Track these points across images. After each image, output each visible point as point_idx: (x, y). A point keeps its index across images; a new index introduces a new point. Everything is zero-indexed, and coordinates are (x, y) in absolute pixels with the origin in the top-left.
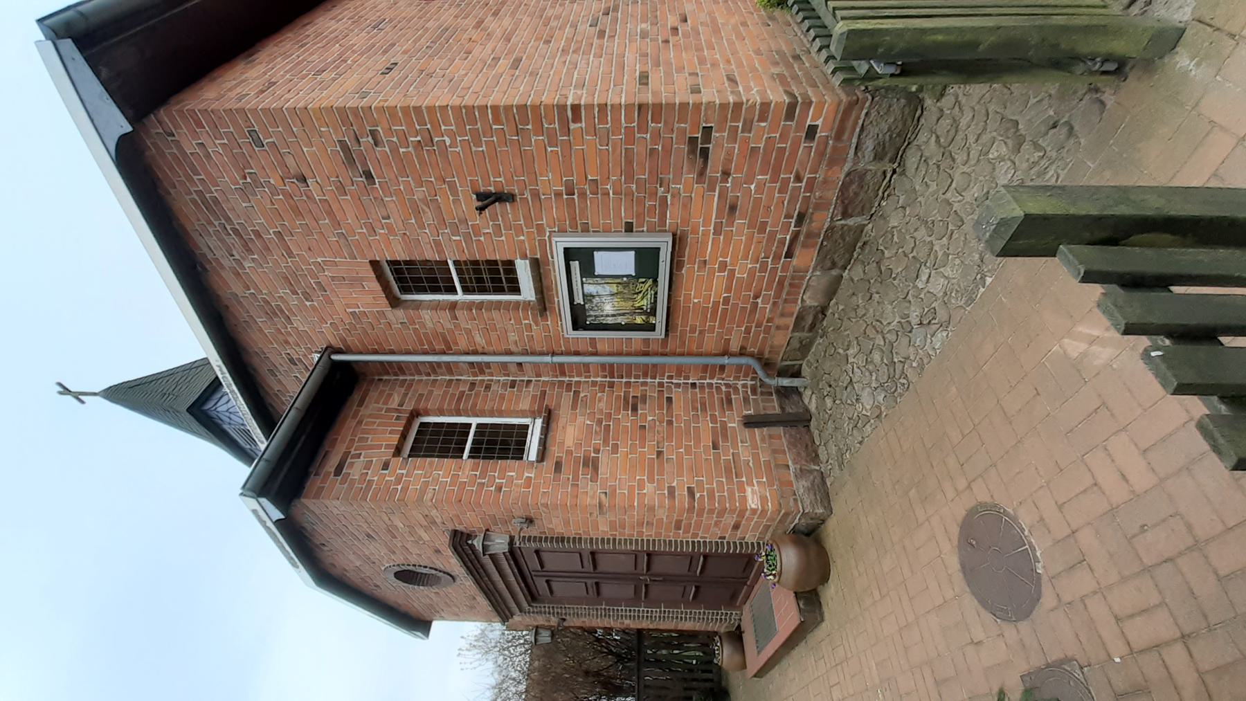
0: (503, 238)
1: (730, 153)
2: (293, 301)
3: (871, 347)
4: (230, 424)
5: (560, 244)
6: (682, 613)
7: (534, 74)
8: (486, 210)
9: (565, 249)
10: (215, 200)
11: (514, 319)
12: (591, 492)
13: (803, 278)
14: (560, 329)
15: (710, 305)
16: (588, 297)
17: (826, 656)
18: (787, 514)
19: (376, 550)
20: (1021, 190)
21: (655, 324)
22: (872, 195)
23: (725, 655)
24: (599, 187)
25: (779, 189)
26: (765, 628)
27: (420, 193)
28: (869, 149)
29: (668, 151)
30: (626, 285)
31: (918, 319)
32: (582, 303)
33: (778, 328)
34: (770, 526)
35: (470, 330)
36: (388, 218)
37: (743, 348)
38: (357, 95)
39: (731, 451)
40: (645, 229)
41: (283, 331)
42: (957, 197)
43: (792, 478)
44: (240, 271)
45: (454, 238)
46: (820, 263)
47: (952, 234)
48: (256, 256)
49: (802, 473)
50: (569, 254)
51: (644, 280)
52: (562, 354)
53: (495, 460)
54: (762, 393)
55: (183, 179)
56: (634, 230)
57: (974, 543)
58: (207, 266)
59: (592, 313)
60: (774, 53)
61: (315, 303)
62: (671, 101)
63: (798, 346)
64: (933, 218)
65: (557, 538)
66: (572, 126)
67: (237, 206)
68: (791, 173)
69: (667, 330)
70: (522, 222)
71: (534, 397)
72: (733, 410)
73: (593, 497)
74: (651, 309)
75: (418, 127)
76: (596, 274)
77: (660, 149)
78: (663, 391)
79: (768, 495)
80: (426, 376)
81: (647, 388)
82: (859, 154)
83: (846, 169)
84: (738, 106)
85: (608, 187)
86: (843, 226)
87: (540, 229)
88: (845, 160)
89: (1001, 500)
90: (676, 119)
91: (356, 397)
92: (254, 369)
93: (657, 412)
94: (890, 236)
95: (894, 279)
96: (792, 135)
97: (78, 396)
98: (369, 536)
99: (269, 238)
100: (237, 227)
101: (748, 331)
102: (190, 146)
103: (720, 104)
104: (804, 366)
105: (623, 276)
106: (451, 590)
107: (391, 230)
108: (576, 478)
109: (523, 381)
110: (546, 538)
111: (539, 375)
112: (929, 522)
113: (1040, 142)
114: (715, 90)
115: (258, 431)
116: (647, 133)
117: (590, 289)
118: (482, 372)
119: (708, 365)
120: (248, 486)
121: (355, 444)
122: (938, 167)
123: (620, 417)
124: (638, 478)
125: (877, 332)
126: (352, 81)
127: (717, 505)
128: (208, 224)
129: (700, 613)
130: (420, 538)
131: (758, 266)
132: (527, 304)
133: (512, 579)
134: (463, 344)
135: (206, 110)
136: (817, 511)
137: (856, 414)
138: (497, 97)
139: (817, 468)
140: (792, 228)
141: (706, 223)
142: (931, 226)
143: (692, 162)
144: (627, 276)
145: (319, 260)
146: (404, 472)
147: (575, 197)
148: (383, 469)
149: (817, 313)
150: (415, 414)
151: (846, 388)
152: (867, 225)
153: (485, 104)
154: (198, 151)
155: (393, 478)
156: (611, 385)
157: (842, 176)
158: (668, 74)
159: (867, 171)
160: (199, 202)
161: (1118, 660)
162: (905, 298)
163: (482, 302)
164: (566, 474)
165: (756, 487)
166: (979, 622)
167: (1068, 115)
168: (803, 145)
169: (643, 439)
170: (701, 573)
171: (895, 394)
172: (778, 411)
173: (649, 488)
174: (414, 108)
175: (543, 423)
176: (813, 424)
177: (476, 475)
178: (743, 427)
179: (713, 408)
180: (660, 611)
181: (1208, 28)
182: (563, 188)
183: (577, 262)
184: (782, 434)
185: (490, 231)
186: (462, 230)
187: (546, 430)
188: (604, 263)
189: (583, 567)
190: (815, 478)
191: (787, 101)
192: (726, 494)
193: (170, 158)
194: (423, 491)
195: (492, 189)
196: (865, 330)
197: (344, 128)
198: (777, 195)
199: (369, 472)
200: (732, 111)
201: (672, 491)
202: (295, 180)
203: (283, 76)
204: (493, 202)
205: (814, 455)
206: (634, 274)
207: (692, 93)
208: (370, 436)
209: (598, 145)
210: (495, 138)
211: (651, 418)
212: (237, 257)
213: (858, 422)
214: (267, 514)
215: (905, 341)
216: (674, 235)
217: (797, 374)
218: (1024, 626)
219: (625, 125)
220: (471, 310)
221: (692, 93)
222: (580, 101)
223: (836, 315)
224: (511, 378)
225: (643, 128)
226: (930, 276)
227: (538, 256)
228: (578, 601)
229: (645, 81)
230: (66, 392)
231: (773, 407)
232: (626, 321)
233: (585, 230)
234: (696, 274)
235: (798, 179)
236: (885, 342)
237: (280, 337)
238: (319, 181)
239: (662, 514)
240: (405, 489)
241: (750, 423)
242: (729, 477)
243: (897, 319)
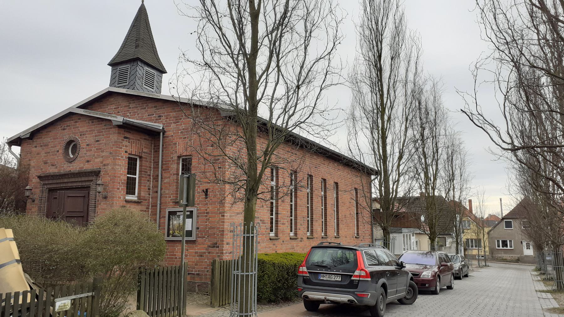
1: (213, 253)
16: (179, 216)
35: (170, 179)
52: (160, 207)
59: (174, 217)
66: (221, 215)
71: (145, 197)
76: (268, 120)
84: (222, 253)
91: (147, 137)
111: (152, 198)
117: (181, 217)
118: (154, 179)
134: (165, 175)
141: (198, 249)
146: (124, 158)
188: (189, 221)
195: (208, 193)
208: (135, 145)
216: (195, 241)
233: (198, 216)
240: (119, 159)
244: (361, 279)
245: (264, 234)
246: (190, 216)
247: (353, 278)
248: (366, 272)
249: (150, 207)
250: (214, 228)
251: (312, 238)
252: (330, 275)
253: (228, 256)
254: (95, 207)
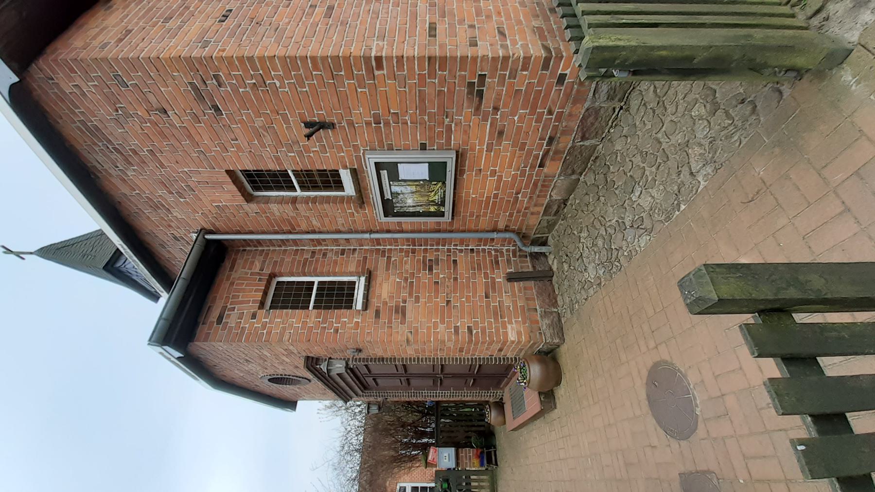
0: (328, 154)
1: (499, 95)
2: (171, 199)
3: (596, 235)
4: (137, 276)
5: (371, 159)
6: (465, 393)
7: (344, 23)
8: (314, 136)
9: (376, 163)
10: (96, 128)
11: (341, 209)
12: (401, 332)
13: (551, 181)
14: (375, 215)
15: (484, 199)
16: (395, 195)
17: (557, 430)
18: (534, 344)
19: (253, 367)
20: (717, 270)
21: (444, 212)
22: (604, 124)
23: (492, 417)
24: (400, 118)
25: (536, 120)
26: (519, 408)
27: (259, 122)
28: (604, 92)
29: (451, 92)
30: (422, 186)
31: (630, 223)
32: (391, 198)
33: (532, 214)
34: (523, 349)
35: (307, 216)
36: (237, 140)
37: (506, 226)
38: (200, 44)
39: (498, 299)
40: (435, 148)
41: (166, 219)
42: (666, 139)
43: (539, 319)
44: (126, 178)
45: (290, 154)
46: (564, 172)
47: (659, 166)
48: (136, 168)
49: (545, 314)
50: (379, 166)
51: (435, 183)
52: (377, 232)
53: (333, 310)
54: (520, 256)
55: (67, 111)
56: (427, 148)
57: (657, 384)
58: (99, 175)
59: (398, 205)
60: (535, 4)
61: (188, 200)
62: (454, 55)
63: (546, 225)
64: (647, 150)
65: (379, 359)
66: (377, 73)
67: (114, 132)
68: (545, 109)
69: (453, 215)
70: (342, 143)
72: (499, 269)
73: (402, 335)
74: (441, 202)
75: (252, 73)
76: (400, 179)
77: (446, 90)
78: (450, 255)
79: (522, 330)
80: (278, 247)
81: (439, 253)
82: (596, 95)
83: (587, 105)
84: (506, 59)
85: (407, 118)
86: (581, 146)
87: (356, 148)
88: (585, 100)
89: (678, 364)
90: (458, 69)
91: (227, 264)
92: (148, 244)
93: (446, 271)
94: (615, 157)
95: (616, 189)
96: (547, 81)
97: (18, 254)
98: (247, 360)
99: (144, 155)
100: (117, 146)
101: (511, 215)
102: (68, 88)
103: (492, 58)
104: (550, 238)
105: (421, 180)
106: (309, 386)
107: (239, 147)
108: (390, 322)
109: (350, 249)
110: (372, 359)
112: (628, 363)
113: (730, 112)
114: (488, 43)
115: (158, 285)
116: (435, 79)
119: (482, 239)
120: (153, 339)
121: (230, 300)
122: (654, 112)
123: (421, 275)
124: (433, 320)
125: (601, 225)
126: (194, 28)
127: (487, 339)
128: (93, 144)
129: (476, 393)
130: (284, 361)
131: (519, 172)
132: (350, 198)
133: (350, 380)
134: (304, 226)
135: (76, 59)
136: (555, 341)
137: (584, 279)
138: (314, 48)
139: (556, 310)
140: (544, 147)
142: (645, 156)
143: (470, 100)
144: (423, 180)
145: (185, 170)
146: (267, 320)
147: (382, 125)
148: (252, 319)
149: (561, 203)
150: (272, 276)
151: (578, 260)
152: (598, 145)
153: (305, 55)
154: (75, 90)
155: (260, 325)
156: (414, 251)
157: (583, 111)
158: (452, 26)
159: (601, 107)
160: (84, 129)
161: (742, 481)
162: (623, 205)
163: (316, 197)
164: (384, 319)
165: (514, 325)
166: (656, 434)
167: (753, 96)
168: (554, 88)
169: (437, 291)
170: (477, 372)
171: (612, 272)
172: (531, 269)
173: (441, 328)
174: (248, 58)
175: (366, 279)
176: (555, 279)
177: (319, 321)
179: (485, 267)
180: (451, 393)
181: (870, 55)
182: (372, 119)
183: (386, 171)
184: (533, 286)
185: (318, 149)
186: (295, 148)
187: (368, 287)
188: (405, 172)
189: (397, 371)
190: (554, 317)
191: (544, 56)
192: (493, 330)
193: (53, 96)
194: (282, 334)
196: (593, 222)
197: (192, 74)
198: (534, 124)
199: (242, 321)
200: (502, 63)
201: (457, 329)
202: (157, 112)
203: (137, 23)
204: (318, 130)
205: (554, 301)
206: (428, 179)
207: (470, 46)
208: (241, 294)
209: (398, 88)
210: (315, 82)
211: (442, 276)
212: (121, 168)
213: (585, 285)
214: (170, 354)
215: (620, 236)
216: (457, 152)
217: (544, 243)
218: (684, 443)
219: (418, 73)
220: (308, 203)
221: (470, 46)
222: (382, 52)
223: (574, 206)
224: (341, 248)
225: (432, 74)
226: (641, 193)
227: (356, 167)
228: (396, 388)
229: (433, 33)
230: (9, 252)
231: (528, 266)
232: (423, 210)
233: (391, 148)
234: (474, 178)
235: (550, 113)
236: (606, 233)
237: (164, 222)
238: (177, 112)
239: (450, 345)
240: (269, 333)
241: (511, 278)
242: (496, 319)
243: (616, 219)
246: (392, 169)
249: (382, 247)
254: (383, 359)
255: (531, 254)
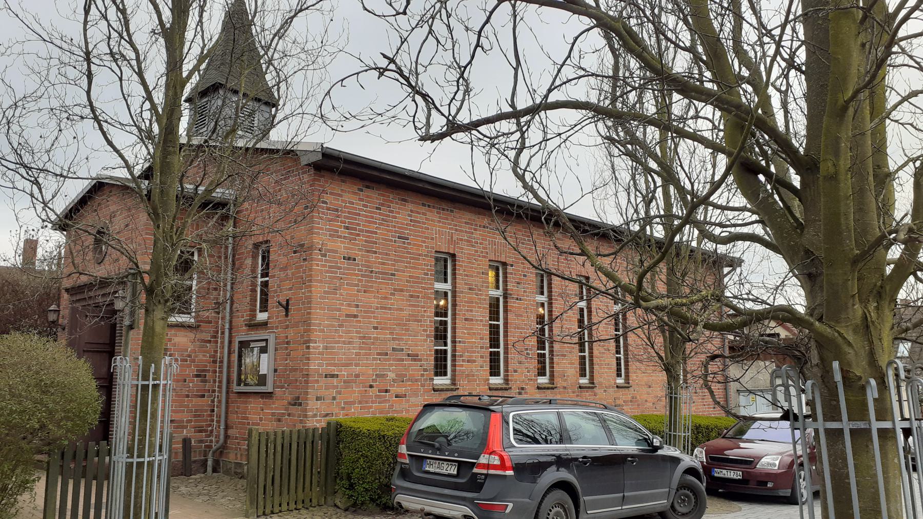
16: (252, 349)
54: (205, 451)
84: (306, 416)
117: (256, 350)
132: (255, 316)
141: (276, 408)
163: (256, 291)
174: (311, 280)
178: (183, 438)
179: (196, 421)
188: (264, 357)
217: (215, 470)
229: (328, 376)
231: (196, 457)
233: (276, 350)
241: (186, 442)
244: (492, 472)
245: (417, 380)
246: (264, 350)
247: (475, 470)
248: (502, 458)
249: (219, 335)
250: (295, 370)
251: (552, 388)
252: (441, 462)
253: (318, 421)
255: (206, 460)
